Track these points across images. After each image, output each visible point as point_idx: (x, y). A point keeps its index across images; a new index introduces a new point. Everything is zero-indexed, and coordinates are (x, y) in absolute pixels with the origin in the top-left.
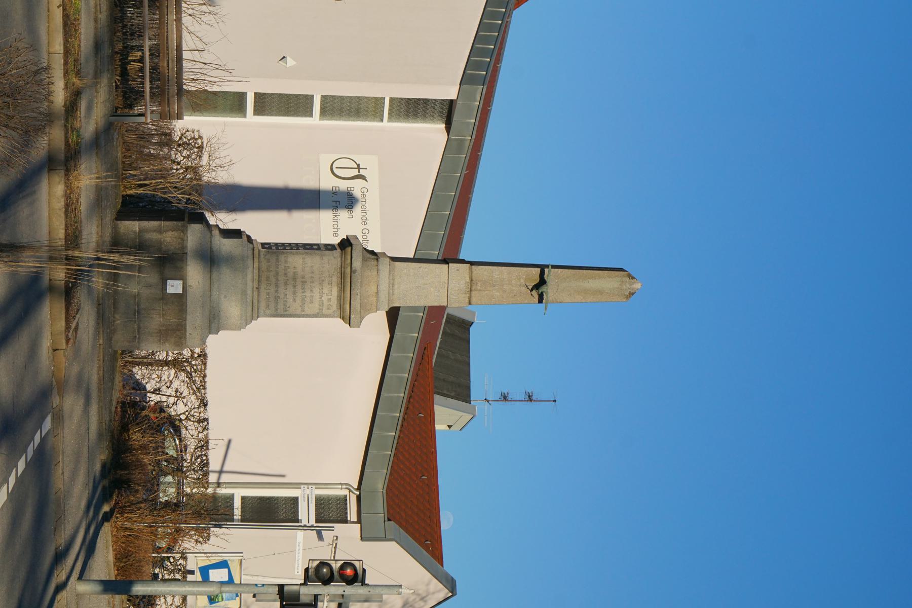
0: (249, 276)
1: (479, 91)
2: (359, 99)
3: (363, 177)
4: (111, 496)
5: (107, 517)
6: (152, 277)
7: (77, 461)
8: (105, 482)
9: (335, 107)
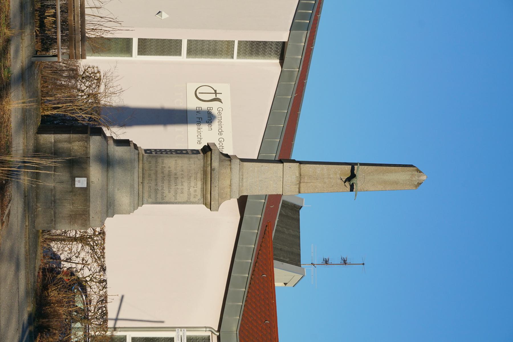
1: (304, 35)
2: (216, 42)
3: (219, 100)
6: (63, 175)
8: (32, 328)
9: (198, 48)
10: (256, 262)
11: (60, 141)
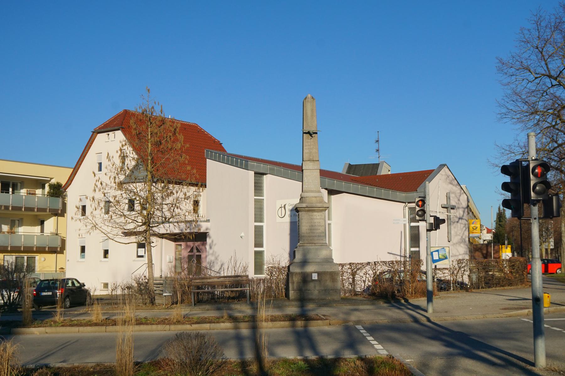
0: (310, 247)
1: (250, 163)
2: (255, 208)
3: (285, 206)
4: (399, 299)
5: (406, 301)
6: (311, 285)
7: (379, 314)
8: (392, 302)
9: (259, 216)
10: (367, 184)
11: (293, 288)
